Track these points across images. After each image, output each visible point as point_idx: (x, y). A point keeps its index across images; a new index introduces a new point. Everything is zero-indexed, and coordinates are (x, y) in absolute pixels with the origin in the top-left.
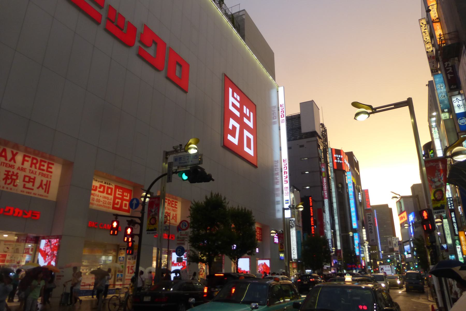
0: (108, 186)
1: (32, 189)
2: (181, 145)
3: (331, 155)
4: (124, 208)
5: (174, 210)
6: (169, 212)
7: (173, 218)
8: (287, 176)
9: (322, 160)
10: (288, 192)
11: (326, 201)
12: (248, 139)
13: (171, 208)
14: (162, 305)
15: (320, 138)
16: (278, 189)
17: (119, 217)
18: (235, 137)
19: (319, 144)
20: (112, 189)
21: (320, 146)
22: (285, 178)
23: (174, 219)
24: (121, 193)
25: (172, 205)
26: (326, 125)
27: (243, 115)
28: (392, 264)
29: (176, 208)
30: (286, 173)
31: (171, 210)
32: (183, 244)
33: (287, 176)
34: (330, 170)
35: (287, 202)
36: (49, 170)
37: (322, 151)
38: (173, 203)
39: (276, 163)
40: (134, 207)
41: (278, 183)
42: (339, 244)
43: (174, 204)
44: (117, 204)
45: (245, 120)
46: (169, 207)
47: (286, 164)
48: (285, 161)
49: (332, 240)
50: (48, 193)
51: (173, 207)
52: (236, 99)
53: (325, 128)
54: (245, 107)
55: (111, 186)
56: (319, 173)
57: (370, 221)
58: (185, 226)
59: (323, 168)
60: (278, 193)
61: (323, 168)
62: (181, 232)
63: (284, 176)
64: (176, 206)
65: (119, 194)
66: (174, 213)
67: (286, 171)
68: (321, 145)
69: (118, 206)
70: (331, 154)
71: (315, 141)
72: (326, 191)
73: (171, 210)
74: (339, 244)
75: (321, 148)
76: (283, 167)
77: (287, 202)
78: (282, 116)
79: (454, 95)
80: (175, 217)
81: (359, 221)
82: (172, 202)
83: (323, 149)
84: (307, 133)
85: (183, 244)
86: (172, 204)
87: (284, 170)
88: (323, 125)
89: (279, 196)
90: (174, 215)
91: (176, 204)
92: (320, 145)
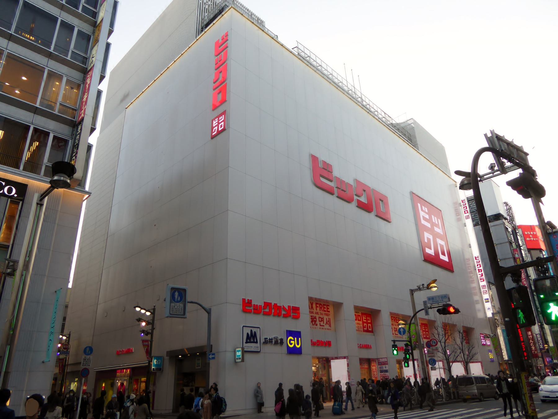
0: (358, 314)
1: (324, 326)
3: (523, 237)
4: (369, 329)
5: (327, 315)
6: (322, 317)
7: (327, 323)
8: (482, 274)
9: (513, 244)
10: (486, 290)
13: (324, 312)
14: (497, 390)
15: (506, 219)
16: (474, 288)
17: (396, 342)
18: (431, 249)
19: (507, 227)
20: (360, 316)
21: (508, 228)
22: (481, 276)
23: (328, 324)
24: (365, 318)
25: (324, 309)
26: (510, 203)
27: (433, 224)
28: (371, 388)
30: (480, 271)
31: (324, 314)
32: (434, 356)
33: (482, 274)
34: (525, 254)
36: (328, 310)
37: (511, 233)
39: (467, 262)
40: (402, 334)
41: (474, 282)
42: (550, 338)
43: (326, 308)
44: (365, 327)
45: (436, 229)
46: (321, 312)
47: (479, 261)
48: (477, 259)
49: (540, 334)
50: (331, 327)
51: (325, 311)
52: (424, 212)
53: (509, 206)
54: (433, 217)
55: (359, 314)
58: (435, 343)
59: (516, 254)
60: (476, 292)
61: (516, 254)
62: (432, 348)
63: (479, 274)
65: (364, 319)
67: (480, 268)
68: (509, 228)
69: (366, 329)
70: (522, 235)
71: (502, 224)
72: (524, 280)
73: (324, 314)
74: (550, 338)
75: (510, 230)
78: (466, 212)
80: (329, 321)
82: (324, 306)
83: (512, 232)
85: (434, 356)
86: (397, 320)
87: (478, 268)
88: (506, 204)
89: (477, 295)
90: (328, 320)
91: (328, 307)
92: (508, 228)
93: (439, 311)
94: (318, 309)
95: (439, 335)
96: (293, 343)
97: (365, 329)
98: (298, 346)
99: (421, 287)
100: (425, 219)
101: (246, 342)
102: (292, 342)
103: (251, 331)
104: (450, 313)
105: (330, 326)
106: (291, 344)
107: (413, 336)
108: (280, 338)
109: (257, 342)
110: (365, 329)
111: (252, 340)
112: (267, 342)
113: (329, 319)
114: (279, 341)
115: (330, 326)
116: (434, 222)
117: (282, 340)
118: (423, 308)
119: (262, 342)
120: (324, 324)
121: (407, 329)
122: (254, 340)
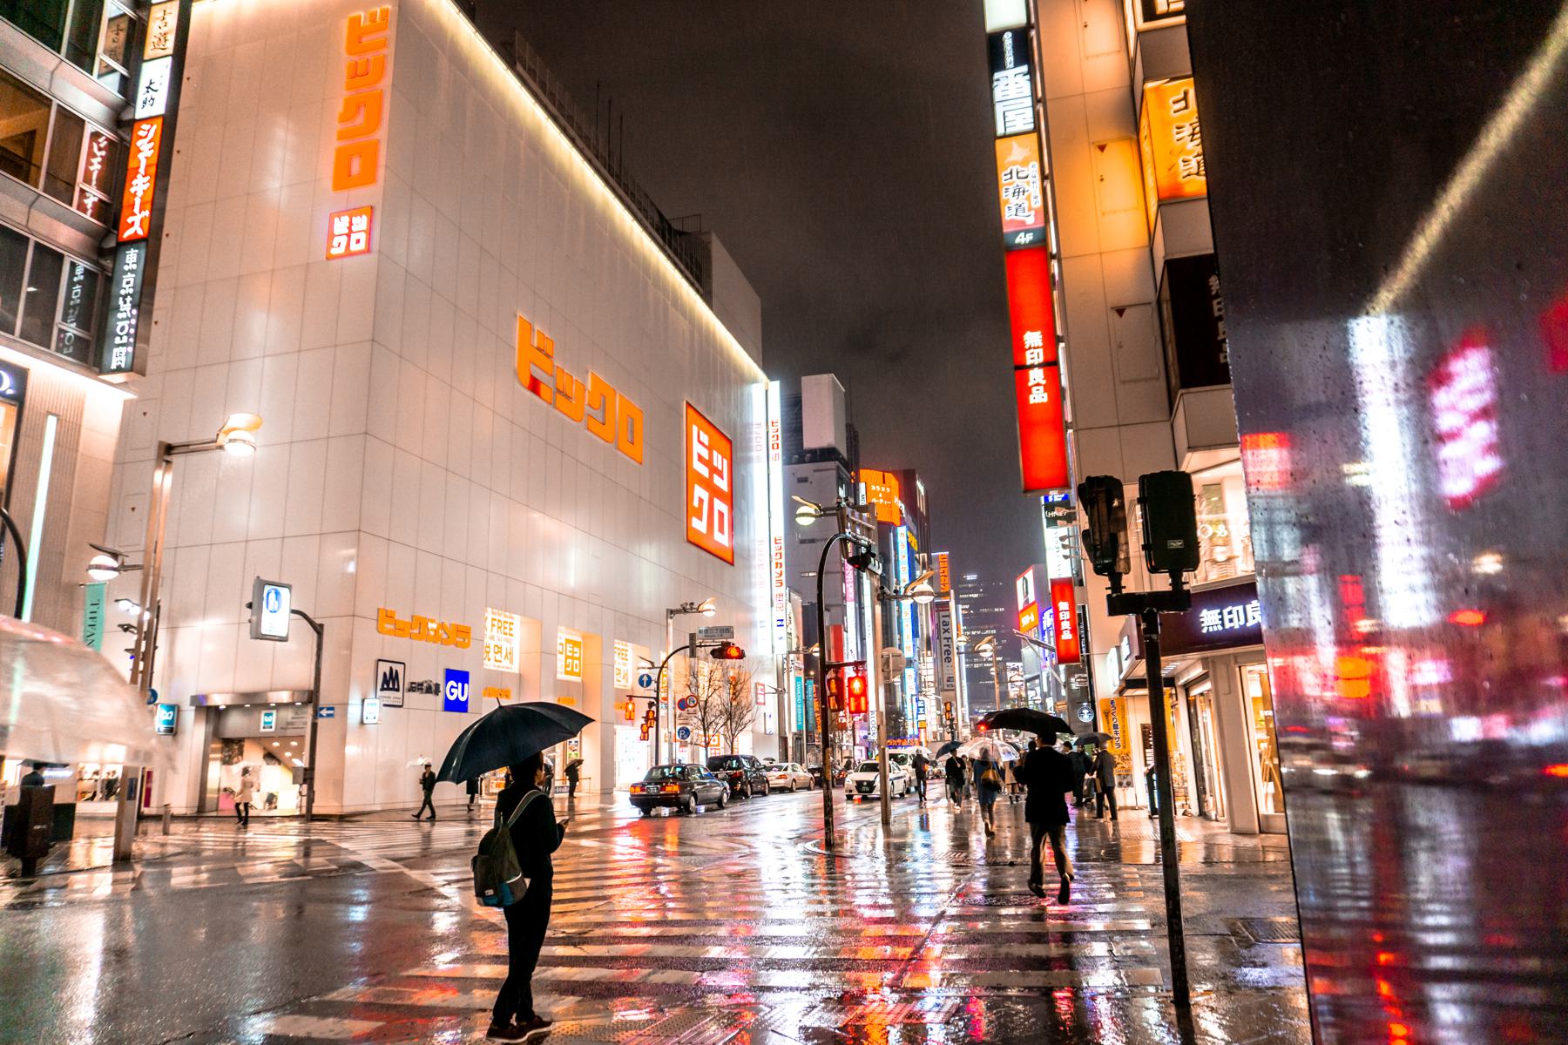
2: (692, 604)
11: (851, 607)
12: (721, 514)
29: (511, 635)
35: (780, 623)
38: (496, 623)
45: (717, 480)
51: (505, 634)
56: (839, 576)
57: (946, 631)
64: (512, 632)
66: (509, 646)
76: (773, 553)
77: (780, 623)
78: (775, 446)
79: (1142, 307)
81: (918, 640)
84: (813, 452)
86: (505, 628)
93: (713, 653)
94: (495, 629)
95: (698, 687)
96: (455, 692)
97: (568, 669)
98: (463, 699)
99: (688, 607)
100: (700, 458)
101: (383, 689)
102: (453, 690)
103: (391, 669)
104: (730, 657)
105: (511, 662)
106: (452, 694)
107: (1126, 767)
108: (435, 682)
109: (398, 690)
110: (568, 669)
111: (391, 686)
112: (416, 687)
113: (512, 649)
114: (433, 688)
115: (511, 662)
116: (701, 432)
117: (437, 686)
118: (688, 644)
119: (407, 686)
120: (502, 659)
121: (654, 677)
122: (394, 685)
